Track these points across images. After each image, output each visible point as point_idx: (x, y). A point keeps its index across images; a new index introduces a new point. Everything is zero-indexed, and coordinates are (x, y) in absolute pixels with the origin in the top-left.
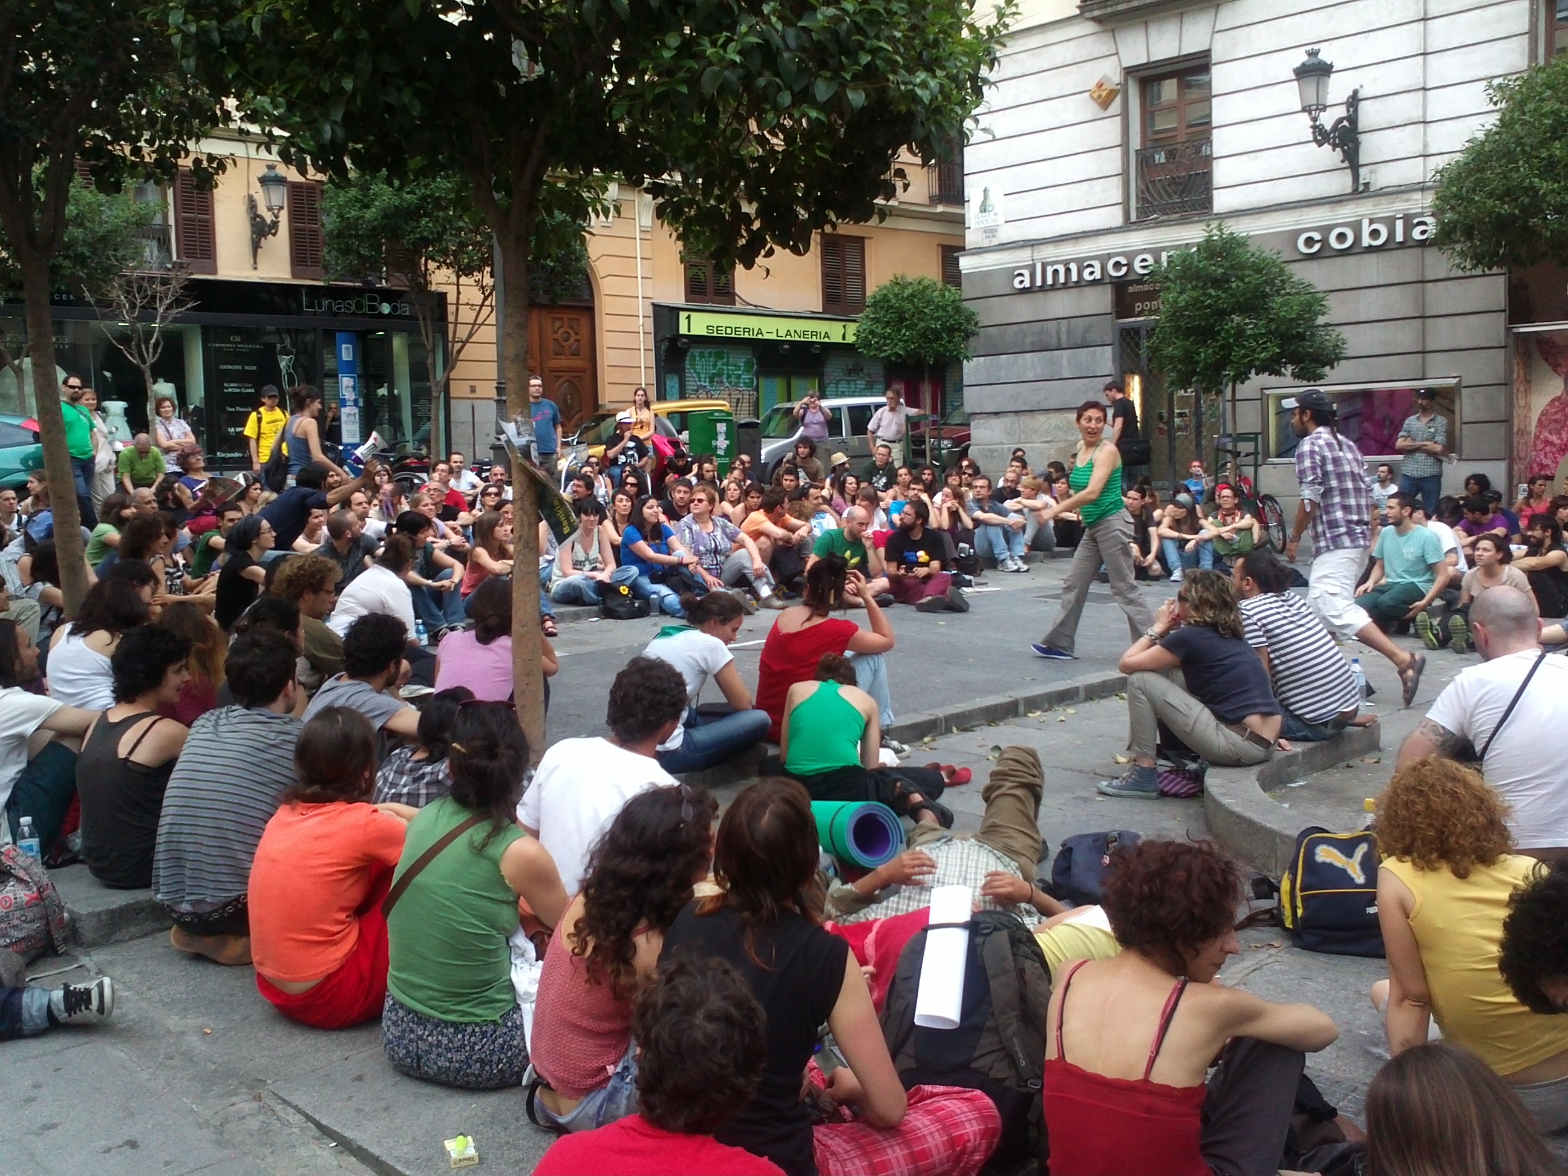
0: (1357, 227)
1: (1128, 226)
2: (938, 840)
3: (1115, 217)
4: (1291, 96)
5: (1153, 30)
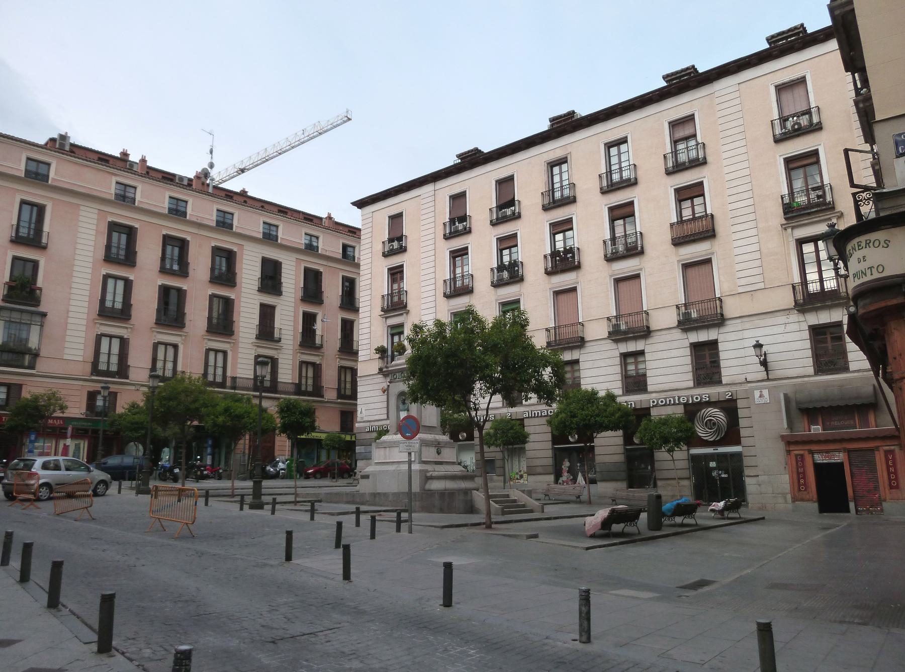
0: (674, 398)
1: (694, 387)
2: (496, 643)
3: (691, 384)
4: (752, 351)
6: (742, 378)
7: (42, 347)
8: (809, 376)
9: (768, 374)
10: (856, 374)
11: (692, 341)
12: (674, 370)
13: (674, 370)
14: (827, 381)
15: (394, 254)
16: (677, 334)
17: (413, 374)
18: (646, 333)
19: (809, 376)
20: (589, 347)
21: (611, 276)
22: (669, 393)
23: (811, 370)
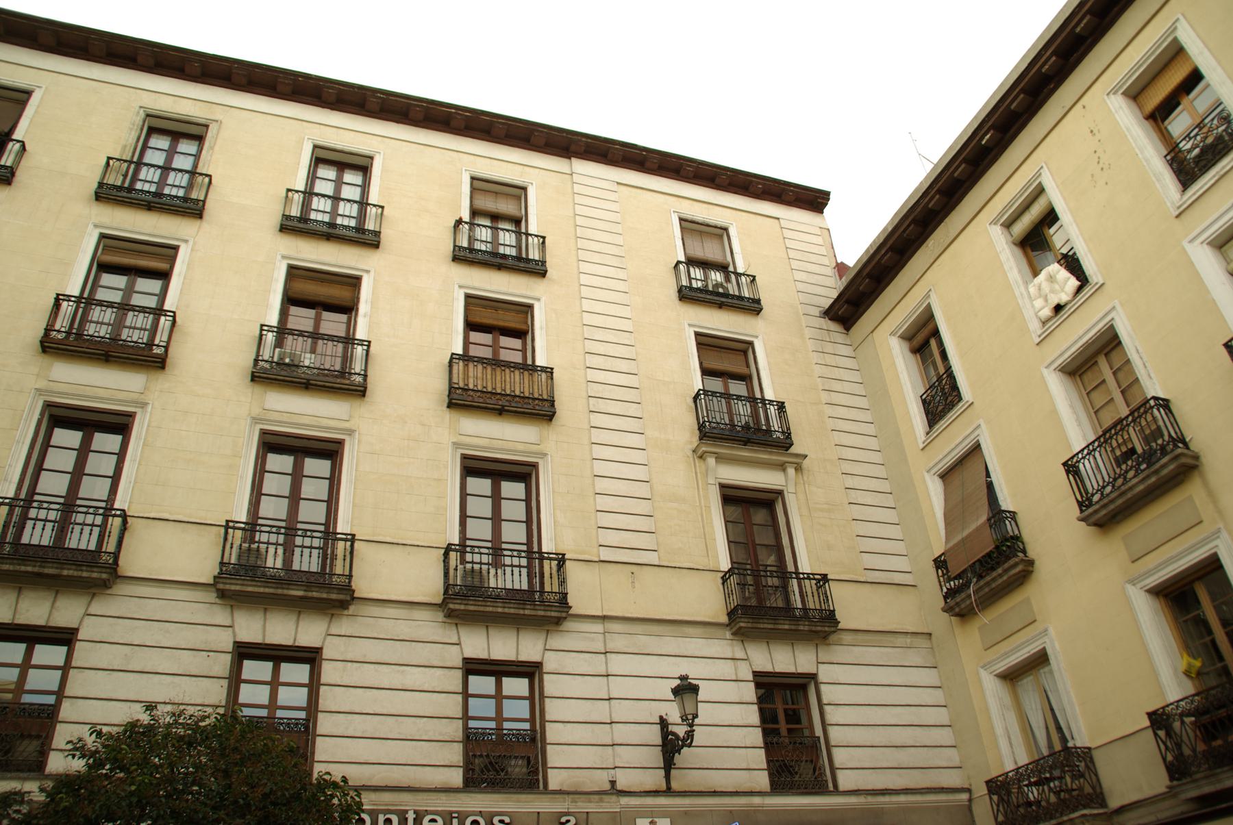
3: (456, 777)
5: (491, 631)
6: (600, 780)
7: (548, 259)
8: (760, 793)
9: (668, 777)
10: (853, 800)
11: (470, 653)
13: (409, 728)
14: (798, 811)
15: (499, 267)
16: (429, 626)
17: (20, 589)
18: (331, 595)
19: (760, 793)
21: (256, 420)
22: (387, 797)
23: (762, 780)
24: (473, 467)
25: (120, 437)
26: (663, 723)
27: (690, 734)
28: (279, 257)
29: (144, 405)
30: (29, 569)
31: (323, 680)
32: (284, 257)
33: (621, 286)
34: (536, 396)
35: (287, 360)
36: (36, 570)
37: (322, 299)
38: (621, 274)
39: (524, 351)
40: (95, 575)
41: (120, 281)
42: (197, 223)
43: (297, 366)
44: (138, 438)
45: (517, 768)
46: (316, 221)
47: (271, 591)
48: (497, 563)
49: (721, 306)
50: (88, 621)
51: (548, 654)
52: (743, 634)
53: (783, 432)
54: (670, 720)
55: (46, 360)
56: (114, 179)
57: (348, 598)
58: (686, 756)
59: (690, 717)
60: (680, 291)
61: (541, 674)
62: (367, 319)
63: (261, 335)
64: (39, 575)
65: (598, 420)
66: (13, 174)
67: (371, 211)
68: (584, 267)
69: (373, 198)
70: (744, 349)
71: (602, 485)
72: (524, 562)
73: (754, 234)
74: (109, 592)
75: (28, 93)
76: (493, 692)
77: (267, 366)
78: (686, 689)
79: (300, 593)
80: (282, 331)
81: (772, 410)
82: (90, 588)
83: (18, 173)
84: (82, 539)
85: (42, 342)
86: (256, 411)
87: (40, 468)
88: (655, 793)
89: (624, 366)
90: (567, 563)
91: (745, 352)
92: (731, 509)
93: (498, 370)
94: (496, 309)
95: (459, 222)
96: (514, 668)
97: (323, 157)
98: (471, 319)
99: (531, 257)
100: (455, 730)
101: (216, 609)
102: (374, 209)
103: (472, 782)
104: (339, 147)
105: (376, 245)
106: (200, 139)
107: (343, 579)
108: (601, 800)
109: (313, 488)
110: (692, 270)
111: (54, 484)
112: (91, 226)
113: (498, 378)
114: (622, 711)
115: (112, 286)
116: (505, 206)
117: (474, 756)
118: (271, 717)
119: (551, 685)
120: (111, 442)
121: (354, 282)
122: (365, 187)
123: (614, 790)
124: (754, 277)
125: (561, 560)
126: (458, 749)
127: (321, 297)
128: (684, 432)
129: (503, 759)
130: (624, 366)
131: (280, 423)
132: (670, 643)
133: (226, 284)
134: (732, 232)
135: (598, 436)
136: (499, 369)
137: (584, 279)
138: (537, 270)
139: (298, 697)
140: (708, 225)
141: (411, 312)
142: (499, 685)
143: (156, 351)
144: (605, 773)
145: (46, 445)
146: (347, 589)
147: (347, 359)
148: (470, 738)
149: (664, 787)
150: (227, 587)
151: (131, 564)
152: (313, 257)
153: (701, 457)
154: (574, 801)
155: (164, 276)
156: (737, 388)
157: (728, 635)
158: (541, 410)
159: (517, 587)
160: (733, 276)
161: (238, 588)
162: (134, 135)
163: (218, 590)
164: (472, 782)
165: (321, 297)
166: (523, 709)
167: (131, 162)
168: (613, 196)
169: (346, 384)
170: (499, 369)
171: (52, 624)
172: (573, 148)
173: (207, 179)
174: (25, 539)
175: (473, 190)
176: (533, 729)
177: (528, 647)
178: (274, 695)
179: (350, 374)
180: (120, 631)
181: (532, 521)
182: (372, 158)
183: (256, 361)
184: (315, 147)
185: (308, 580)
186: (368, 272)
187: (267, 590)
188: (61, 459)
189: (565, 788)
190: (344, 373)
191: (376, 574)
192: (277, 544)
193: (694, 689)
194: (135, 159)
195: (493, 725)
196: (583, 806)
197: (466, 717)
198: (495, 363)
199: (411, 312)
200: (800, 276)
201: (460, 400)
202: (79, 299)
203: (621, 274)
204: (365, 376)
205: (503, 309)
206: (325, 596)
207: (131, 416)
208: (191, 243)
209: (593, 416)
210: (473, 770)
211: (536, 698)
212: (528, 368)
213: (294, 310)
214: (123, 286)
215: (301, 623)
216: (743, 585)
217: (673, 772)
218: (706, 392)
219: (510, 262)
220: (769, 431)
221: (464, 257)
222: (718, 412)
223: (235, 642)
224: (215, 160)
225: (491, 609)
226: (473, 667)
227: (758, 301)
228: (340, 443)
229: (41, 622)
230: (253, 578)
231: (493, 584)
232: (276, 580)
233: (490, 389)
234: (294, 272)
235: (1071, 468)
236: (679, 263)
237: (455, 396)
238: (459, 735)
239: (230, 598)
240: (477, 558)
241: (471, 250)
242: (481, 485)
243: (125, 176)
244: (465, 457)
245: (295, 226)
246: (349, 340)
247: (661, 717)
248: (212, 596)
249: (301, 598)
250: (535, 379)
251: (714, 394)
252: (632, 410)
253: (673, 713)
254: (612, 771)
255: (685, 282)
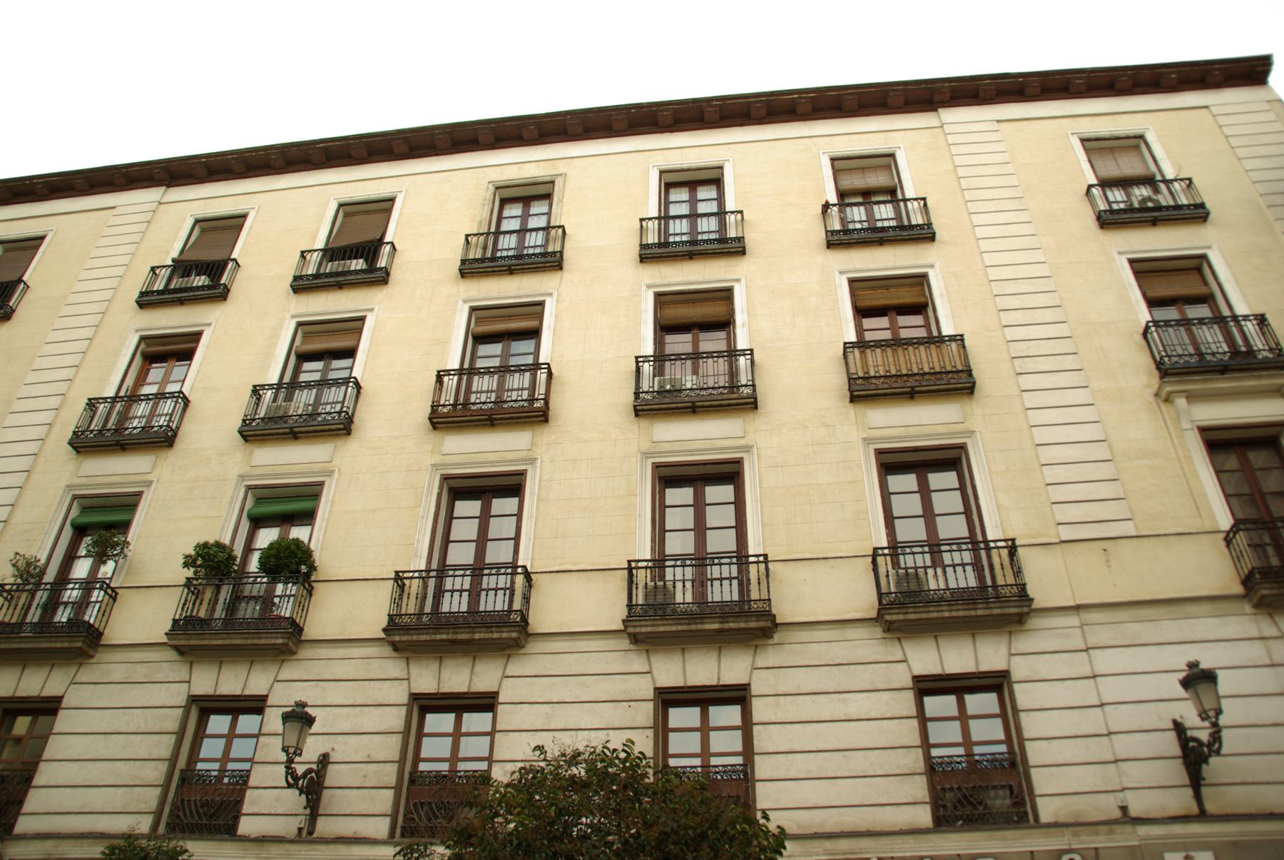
3: (924, 816)
5: (942, 642)
6: (1107, 807)
7: (933, 220)
9: (1198, 797)
11: (920, 669)
12: (859, 763)
13: (859, 763)
16: (868, 645)
18: (752, 624)
20: (108, 667)
21: (646, 455)
24: (892, 462)
25: (516, 500)
26: (1179, 728)
27: (1216, 737)
28: (644, 288)
29: (532, 461)
30: (444, 637)
31: (755, 719)
32: (649, 287)
33: (1026, 229)
34: (949, 368)
35: (668, 387)
36: (450, 637)
37: (695, 319)
38: (1023, 217)
39: (927, 326)
40: (505, 635)
41: (496, 348)
42: (558, 275)
43: (680, 391)
44: (532, 494)
45: (1000, 801)
46: (675, 243)
47: (684, 628)
48: (937, 562)
49: (1154, 223)
50: (507, 683)
51: (1015, 660)
52: (1268, 605)
53: (1271, 350)
54: (1188, 724)
55: (438, 435)
56: (475, 253)
57: (769, 624)
58: (1214, 767)
59: (1212, 714)
60: (1099, 218)
61: (1010, 684)
62: (746, 329)
63: (638, 370)
64: (454, 642)
65: (1027, 382)
66: (388, 274)
67: (731, 219)
68: (977, 219)
69: (730, 206)
70: (1197, 265)
71: (1048, 454)
72: (967, 557)
73: (1177, 136)
74: (523, 651)
75: (392, 200)
76: (698, 724)
77: (648, 397)
78: (1198, 679)
79: (716, 626)
80: (660, 358)
81: (1250, 327)
82: (504, 649)
83: (392, 273)
84: (493, 603)
85: (430, 419)
86: (646, 446)
87: (447, 541)
88: (1184, 819)
89: (1048, 316)
90: (1019, 549)
91: (1199, 270)
92: (1221, 457)
93: (900, 350)
94: (887, 288)
95: (826, 206)
96: (975, 682)
97: (672, 181)
98: (861, 304)
99: (914, 222)
100: (915, 760)
101: (632, 655)
102: (915, 203)
103: (943, 821)
104: (686, 166)
105: (742, 252)
106: (548, 197)
107: (760, 604)
108: (1112, 832)
109: (720, 516)
110: (1109, 194)
111: (679, 544)
112: (460, 303)
113: (902, 358)
114: (1119, 718)
115: (491, 354)
116: (876, 180)
117: (944, 789)
118: (453, 770)
119: (1024, 696)
120: (509, 504)
121: (726, 295)
122: (721, 199)
123: (1126, 817)
124: (1190, 179)
125: (1013, 549)
126: (922, 782)
127: (695, 320)
128: (1137, 373)
129: (978, 791)
130: (1048, 316)
131: (492, 463)
132: (1170, 628)
133: (597, 324)
134: (1150, 137)
135: (1030, 400)
136: (902, 352)
137: (980, 232)
138: (924, 235)
139: (733, 741)
140: (1118, 138)
141: (794, 309)
142: (961, 705)
143: (537, 405)
144: (1111, 797)
145: (450, 517)
146: (768, 615)
147: (733, 373)
148: (933, 769)
149: (1195, 809)
150: (638, 630)
151: (541, 620)
152: (679, 279)
153: (1167, 400)
154: (1075, 835)
155: (535, 334)
156: (1202, 311)
157: (1248, 608)
158: (958, 384)
159: (962, 584)
160: (1162, 186)
161: (649, 629)
162: (487, 209)
163: (629, 634)
164: (943, 821)
165: (695, 320)
166: (995, 730)
167: (488, 234)
168: (995, 136)
169: (738, 400)
170: (902, 352)
171: (473, 690)
172: (937, 98)
173: (560, 231)
174: (445, 608)
175: (836, 172)
176: (1011, 751)
177: (986, 654)
178: (705, 742)
179: (738, 387)
180: (539, 690)
181: (971, 510)
182: (721, 168)
183: (637, 394)
184: (662, 172)
185: (725, 611)
186: (551, 294)
187: (680, 628)
188: (465, 529)
189: (1062, 820)
190: (733, 386)
191: (795, 595)
192: (730, 579)
193: (310, 721)
194: (493, 229)
195: (961, 751)
196: (1089, 841)
197: (926, 745)
198: (897, 343)
199: (794, 309)
200: (1249, 164)
201: (863, 392)
202: (460, 372)
203: (1023, 217)
204: (754, 386)
205: (894, 286)
206: (743, 625)
207: (739, 462)
208: (555, 295)
209: (1021, 378)
210: (944, 807)
211: (1009, 714)
212: (936, 340)
213: (669, 338)
214: (499, 352)
215: (723, 660)
216: (1257, 547)
217: (1205, 791)
218: (1156, 323)
219: (891, 233)
220: (1251, 352)
221: (839, 240)
222: (1178, 341)
223: (656, 689)
224: (567, 211)
225: (935, 615)
226: (926, 686)
227: (1202, 206)
228: (739, 462)
229: (463, 689)
230: (663, 617)
231: (933, 585)
232: (690, 617)
233: (894, 372)
234: (662, 299)
235: (256, 391)
236: (1090, 187)
237: (856, 388)
238: (920, 766)
239: (643, 642)
240: (909, 559)
241: (846, 231)
242: (905, 482)
243: (485, 248)
244: (879, 453)
245: (654, 253)
246: (732, 354)
247: (1175, 722)
248: (625, 643)
249: (718, 631)
250: (944, 351)
251: (1167, 323)
252: (1069, 362)
253: (1189, 715)
254: (1120, 795)
255: (1102, 206)
